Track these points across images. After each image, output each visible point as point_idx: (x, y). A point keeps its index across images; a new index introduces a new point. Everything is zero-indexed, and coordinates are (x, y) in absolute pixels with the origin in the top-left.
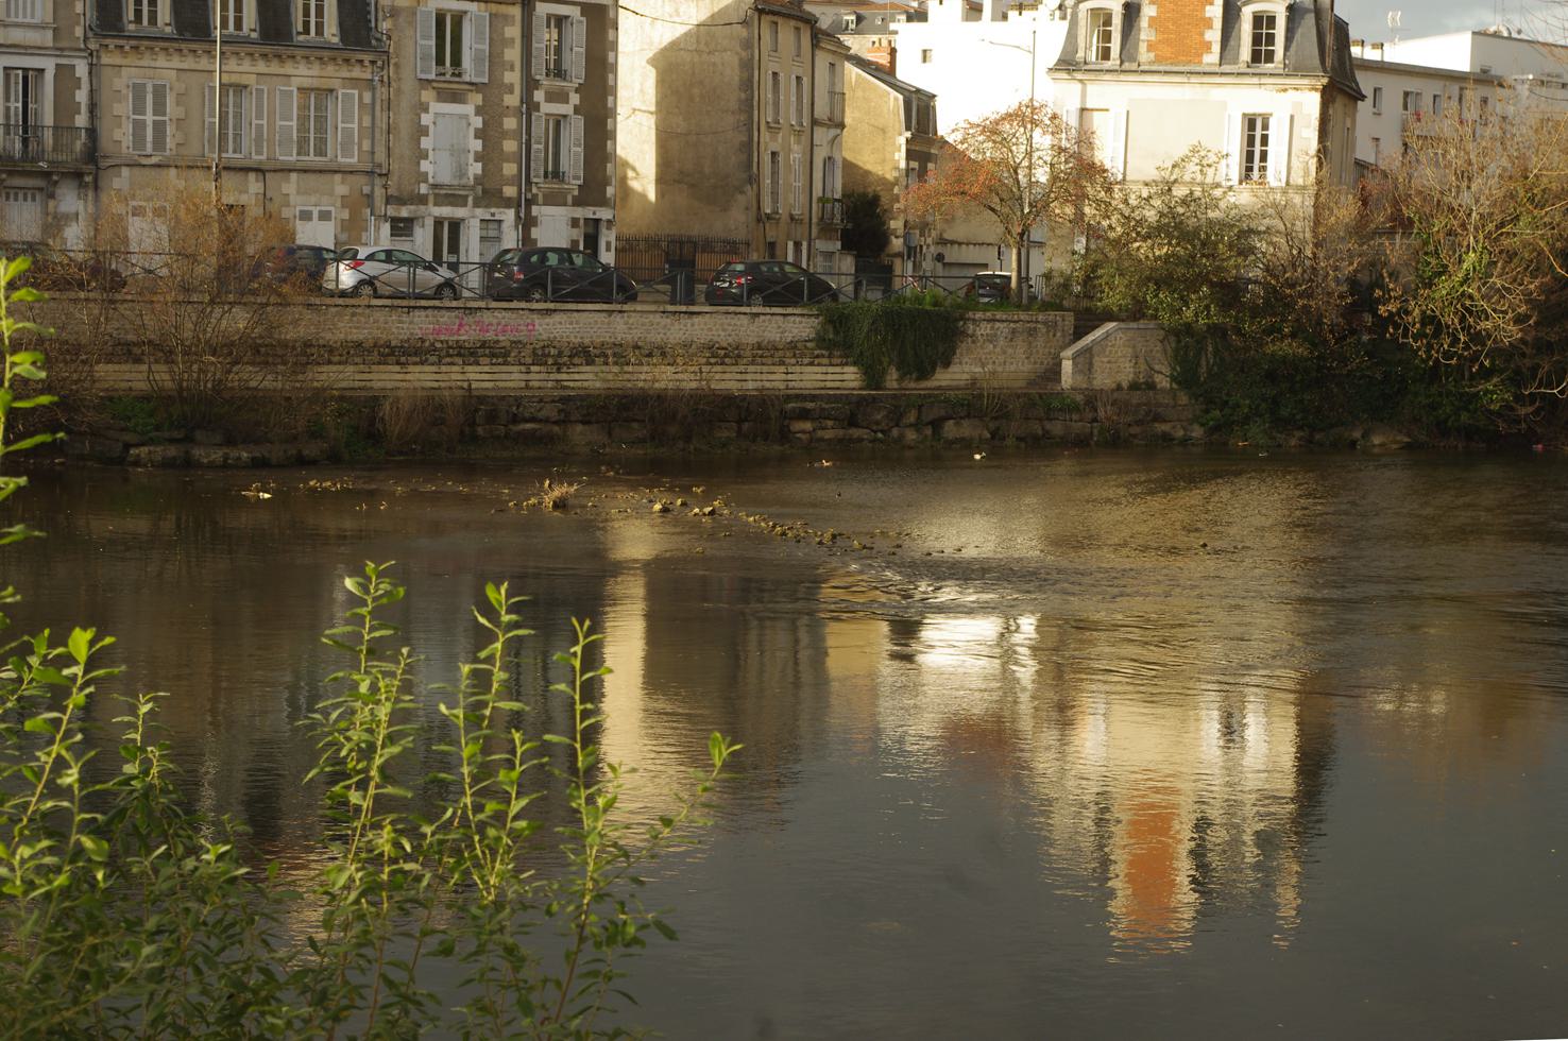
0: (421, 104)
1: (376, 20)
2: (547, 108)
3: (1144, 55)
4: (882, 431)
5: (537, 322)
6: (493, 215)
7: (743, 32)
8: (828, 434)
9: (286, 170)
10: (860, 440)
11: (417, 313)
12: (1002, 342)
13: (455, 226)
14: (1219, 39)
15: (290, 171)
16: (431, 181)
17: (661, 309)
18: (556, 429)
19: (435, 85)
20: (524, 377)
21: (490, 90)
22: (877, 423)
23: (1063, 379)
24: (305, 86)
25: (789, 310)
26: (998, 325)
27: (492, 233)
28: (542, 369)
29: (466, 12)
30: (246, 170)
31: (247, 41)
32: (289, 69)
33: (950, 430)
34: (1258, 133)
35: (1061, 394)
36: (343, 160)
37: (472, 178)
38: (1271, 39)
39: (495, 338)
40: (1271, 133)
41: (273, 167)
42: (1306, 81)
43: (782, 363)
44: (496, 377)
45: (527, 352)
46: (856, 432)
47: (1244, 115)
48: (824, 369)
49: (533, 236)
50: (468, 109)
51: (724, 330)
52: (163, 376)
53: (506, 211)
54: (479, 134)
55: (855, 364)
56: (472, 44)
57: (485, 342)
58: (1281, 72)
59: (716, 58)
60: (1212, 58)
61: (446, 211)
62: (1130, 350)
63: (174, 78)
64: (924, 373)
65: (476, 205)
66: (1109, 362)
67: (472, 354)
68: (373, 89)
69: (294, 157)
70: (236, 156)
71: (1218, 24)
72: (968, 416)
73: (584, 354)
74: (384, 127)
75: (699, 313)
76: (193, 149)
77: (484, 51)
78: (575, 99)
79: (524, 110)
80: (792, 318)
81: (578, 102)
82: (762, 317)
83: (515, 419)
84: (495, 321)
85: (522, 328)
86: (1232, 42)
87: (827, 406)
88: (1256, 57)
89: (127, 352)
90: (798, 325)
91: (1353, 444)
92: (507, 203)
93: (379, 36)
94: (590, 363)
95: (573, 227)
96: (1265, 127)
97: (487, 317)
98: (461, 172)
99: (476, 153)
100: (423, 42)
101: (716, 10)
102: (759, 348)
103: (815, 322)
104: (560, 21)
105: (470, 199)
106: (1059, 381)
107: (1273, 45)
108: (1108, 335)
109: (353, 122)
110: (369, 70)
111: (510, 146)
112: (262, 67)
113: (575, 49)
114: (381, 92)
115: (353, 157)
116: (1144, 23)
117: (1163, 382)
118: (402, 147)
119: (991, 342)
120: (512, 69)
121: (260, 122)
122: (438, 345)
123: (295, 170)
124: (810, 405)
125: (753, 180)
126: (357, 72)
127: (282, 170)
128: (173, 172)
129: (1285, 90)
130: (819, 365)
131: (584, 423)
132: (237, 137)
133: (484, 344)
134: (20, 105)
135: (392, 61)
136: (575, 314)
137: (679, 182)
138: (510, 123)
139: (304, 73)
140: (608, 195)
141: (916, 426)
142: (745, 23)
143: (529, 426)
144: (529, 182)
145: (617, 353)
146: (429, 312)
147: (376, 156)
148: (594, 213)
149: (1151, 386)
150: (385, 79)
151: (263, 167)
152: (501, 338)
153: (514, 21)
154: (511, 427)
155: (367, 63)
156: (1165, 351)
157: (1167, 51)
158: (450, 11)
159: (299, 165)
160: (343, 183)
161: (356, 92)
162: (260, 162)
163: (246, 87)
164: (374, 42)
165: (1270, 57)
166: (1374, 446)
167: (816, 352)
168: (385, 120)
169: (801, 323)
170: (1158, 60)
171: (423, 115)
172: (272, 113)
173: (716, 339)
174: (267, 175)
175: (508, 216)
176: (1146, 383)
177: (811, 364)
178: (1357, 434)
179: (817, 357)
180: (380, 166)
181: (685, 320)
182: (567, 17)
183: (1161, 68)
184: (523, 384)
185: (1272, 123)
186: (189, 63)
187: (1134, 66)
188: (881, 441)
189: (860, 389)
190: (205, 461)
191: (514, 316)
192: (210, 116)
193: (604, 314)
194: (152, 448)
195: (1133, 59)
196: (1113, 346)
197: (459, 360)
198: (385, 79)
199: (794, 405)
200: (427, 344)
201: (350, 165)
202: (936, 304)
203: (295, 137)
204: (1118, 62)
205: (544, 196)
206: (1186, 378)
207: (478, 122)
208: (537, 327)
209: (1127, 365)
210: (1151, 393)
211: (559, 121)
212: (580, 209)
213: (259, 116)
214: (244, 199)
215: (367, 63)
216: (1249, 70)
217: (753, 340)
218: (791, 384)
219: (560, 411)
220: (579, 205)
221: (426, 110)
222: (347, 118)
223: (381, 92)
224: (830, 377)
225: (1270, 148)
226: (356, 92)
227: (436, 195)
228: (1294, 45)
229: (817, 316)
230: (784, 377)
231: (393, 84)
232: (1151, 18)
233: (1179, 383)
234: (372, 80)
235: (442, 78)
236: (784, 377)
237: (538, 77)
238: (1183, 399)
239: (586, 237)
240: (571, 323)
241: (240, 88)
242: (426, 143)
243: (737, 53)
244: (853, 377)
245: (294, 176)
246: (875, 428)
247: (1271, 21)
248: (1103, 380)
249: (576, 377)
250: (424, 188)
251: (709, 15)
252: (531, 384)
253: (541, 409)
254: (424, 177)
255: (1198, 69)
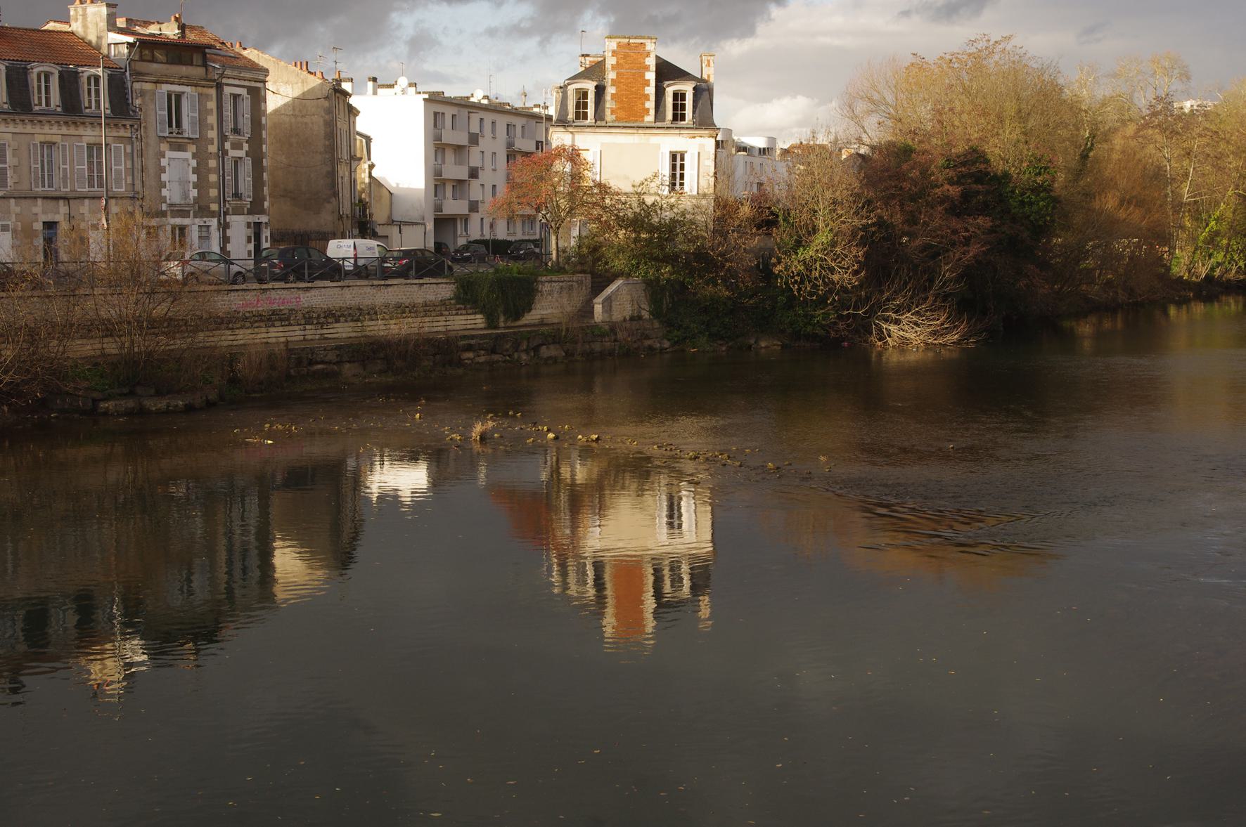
0: (161, 152)
1: (132, 99)
2: (233, 153)
3: (609, 117)
4: (509, 356)
5: (301, 296)
6: (205, 222)
7: (326, 104)
8: (482, 359)
9: (82, 198)
10: (498, 362)
11: (233, 294)
12: (556, 295)
13: (182, 229)
14: (654, 107)
15: (85, 198)
16: (168, 202)
17: (371, 284)
18: (335, 367)
19: (169, 140)
20: (302, 333)
21: (200, 141)
22: (507, 350)
23: (596, 316)
24: (92, 142)
25: (440, 281)
26: (554, 284)
27: (204, 234)
28: (313, 327)
29: (183, 93)
30: (57, 198)
31: (54, 113)
32: (81, 131)
33: (545, 352)
34: (678, 163)
35: (596, 326)
36: (116, 190)
37: (192, 199)
38: (683, 107)
39: (278, 308)
40: (686, 163)
41: (74, 196)
42: (707, 132)
43: (441, 315)
44: (287, 334)
45: (300, 316)
46: (496, 357)
47: (670, 152)
48: (465, 317)
49: (228, 235)
50: (188, 155)
51: (405, 295)
52: (111, 347)
53: (212, 219)
54: (195, 171)
55: (481, 313)
56: (188, 113)
57: (274, 311)
58: (692, 126)
59: (307, 120)
60: (650, 118)
61: (178, 221)
62: (629, 297)
63: (11, 139)
64: (518, 316)
65: (195, 217)
66: (620, 305)
67: (268, 320)
68: (132, 144)
69: (87, 189)
70: (51, 189)
71: (653, 98)
72: (554, 343)
73: (332, 316)
74: (140, 167)
75: (391, 285)
76: (25, 186)
77: (196, 117)
78: (246, 147)
79: (220, 155)
80: (441, 285)
81: (248, 149)
82: (425, 286)
83: (311, 363)
84: (278, 297)
85: (294, 300)
86: (661, 109)
87: (481, 342)
88: (675, 118)
89: (89, 328)
90: (440, 290)
91: (750, 347)
92: (212, 214)
93: (134, 108)
94: (337, 321)
95: (248, 228)
96: (682, 159)
97: (273, 294)
98: (185, 195)
99: (194, 183)
100: (160, 112)
101: (306, 90)
102: (426, 306)
103: (453, 287)
104: (235, 97)
105: (191, 212)
106: (593, 317)
107: (685, 110)
108: (618, 288)
109: (121, 165)
110: (129, 131)
111: (213, 178)
112: (64, 130)
113: (246, 116)
114: (137, 144)
115: (122, 188)
116: (608, 97)
117: (646, 315)
118: (151, 182)
119: (550, 294)
120: (212, 129)
121: (65, 167)
122: (247, 315)
123: (40, 197)
124: (473, 342)
125: (336, 195)
126: (122, 133)
127: (79, 198)
128: (12, 201)
129: (694, 137)
130: (461, 315)
131: (349, 362)
132: (51, 177)
133: (274, 312)
134: (39, 166)
135: (142, 125)
136: (323, 290)
137: (283, 196)
138: (212, 163)
139: (89, 134)
140: (265, 207)
141: (527, 351)
142: (326, 98)
143: (320, 366)
144: (225, 201)
145: (355, 314)
146: (240, 293)
147: (135, 186)
148: (259, 219)
149: (640, 318)
150: (139, 137)
151: (69, 196)
152: (282, 308)
153: (212, 97)
154: (309, 368)
155: (128, 127)
156: (646, 296)
157: (622, 114)
158: (175, 92)
159: (90, 194)
160: (116, 204)
161: (122, 145)
162: (66, 193)
163: (54, 143)
164: (131, 112)
165: (585, 117)
166: (762, 347)
167: (458, 306)
168: (140, 163)
169: (446, 288)
170: (618, 119)
171: (162, 160)
172: (72, 161)
173: (402, 301)
174: (70, 201)
175: (214, 222)
176: (638, 316)
177: (457, 314)
178: (752, 341)
179: (458, 309)
180: (138, 193)
181: (384, 290)
182: (239, 95)
183: (620, 125)
184: (302, 338)
185: (687, 157)
186: (19, 128)
187: (603, 123)
188: (509, 361)
189: (485, 329)
190: (154, 409)
191: (289, 293)
192: (35, 164)
193: (339, 289)
194: (117, 402)
195: (602, 119)
196: (621, 294)
197: (263, 324)
198: (139, 137)
199: (464, 342)
200: (241, 314)
201: (120, 193)
202: (519, 273)
203: (87, 177)
204: (594, 121)
205: (233, 209)
206: (656, 313)
207: (194, 163)
208: (302, 299)
209: (629, 306)
210: (641, 322)
211: (237, 161)
212: (251, 216)
213: (64, 163)
214: (57, 218)
215: (128, 127)
216: (673, 125)
217: (420, 300)
218: (449, 328)
219: (337, 356)
220: (250, 214)
221: (164, 156)
222: (118, 163)
223: (137, 144)
224: (469, 322)
225: (686, 172)
226: (122, 145)
227: (172, 211)
228: (698, 110)
229: (454, 283)
230: (444, 323)
231: (144, 140)
232: (612, 94)
233: (653, 315)
234: (131, 138)
235: (171, 135)
236: (444, 323)
237: (227, 134)
238: (657, 325)
239: (255, 233)
240: (321, 296)
241: (51, 145)
242: (164, 177)
243: (322, 116)
244: (480, 321)
245: (87, 201)
246: (505, 353)
247: (683, 96)
248: (617, 316)
249: (332, 331)
250: (164, 207)
251: (301, 93)
252: (306, 337)
253: (326, 356)
254: (163, 200)
255: (642, 125)
